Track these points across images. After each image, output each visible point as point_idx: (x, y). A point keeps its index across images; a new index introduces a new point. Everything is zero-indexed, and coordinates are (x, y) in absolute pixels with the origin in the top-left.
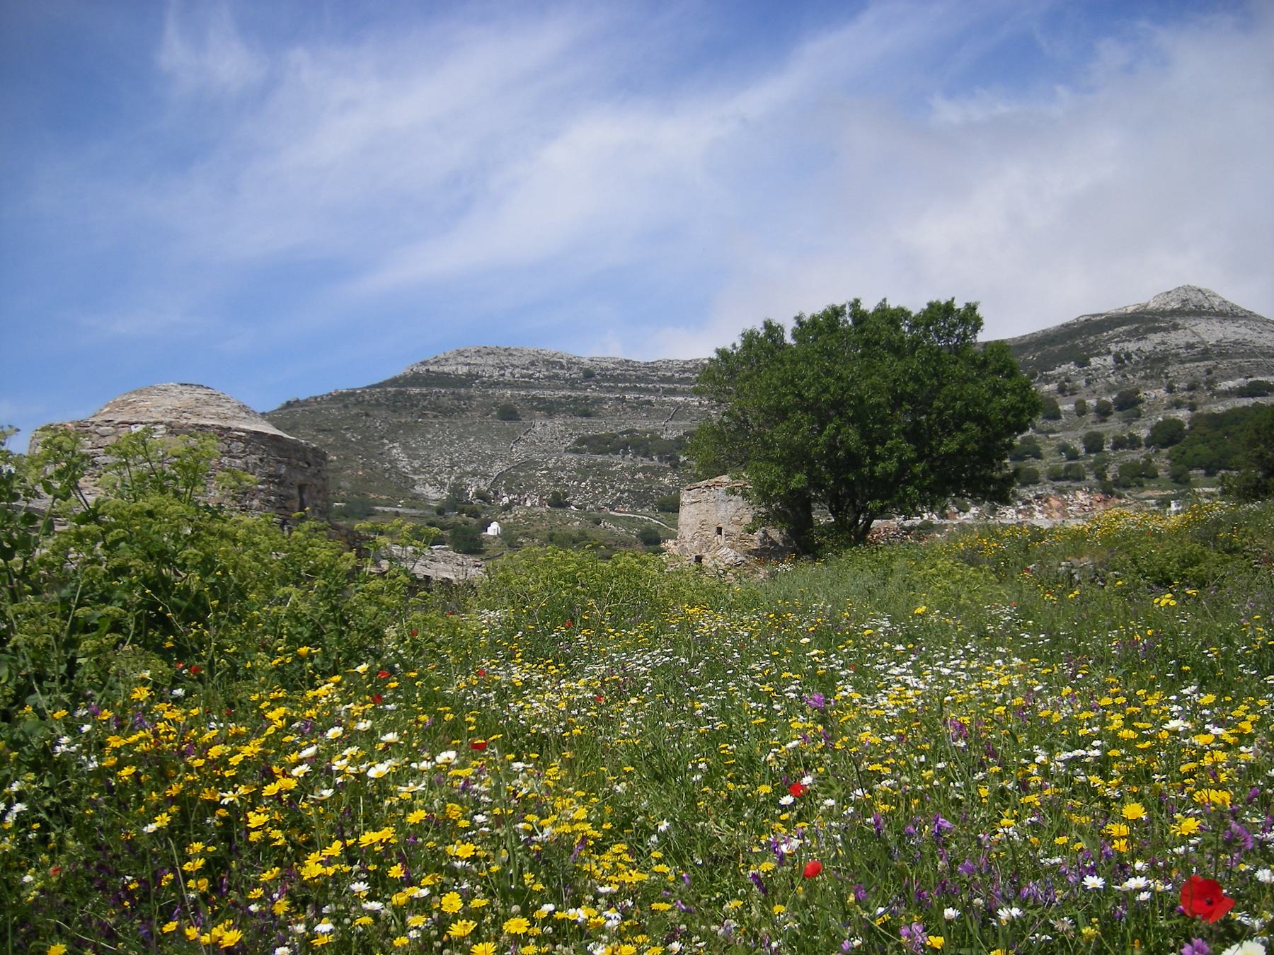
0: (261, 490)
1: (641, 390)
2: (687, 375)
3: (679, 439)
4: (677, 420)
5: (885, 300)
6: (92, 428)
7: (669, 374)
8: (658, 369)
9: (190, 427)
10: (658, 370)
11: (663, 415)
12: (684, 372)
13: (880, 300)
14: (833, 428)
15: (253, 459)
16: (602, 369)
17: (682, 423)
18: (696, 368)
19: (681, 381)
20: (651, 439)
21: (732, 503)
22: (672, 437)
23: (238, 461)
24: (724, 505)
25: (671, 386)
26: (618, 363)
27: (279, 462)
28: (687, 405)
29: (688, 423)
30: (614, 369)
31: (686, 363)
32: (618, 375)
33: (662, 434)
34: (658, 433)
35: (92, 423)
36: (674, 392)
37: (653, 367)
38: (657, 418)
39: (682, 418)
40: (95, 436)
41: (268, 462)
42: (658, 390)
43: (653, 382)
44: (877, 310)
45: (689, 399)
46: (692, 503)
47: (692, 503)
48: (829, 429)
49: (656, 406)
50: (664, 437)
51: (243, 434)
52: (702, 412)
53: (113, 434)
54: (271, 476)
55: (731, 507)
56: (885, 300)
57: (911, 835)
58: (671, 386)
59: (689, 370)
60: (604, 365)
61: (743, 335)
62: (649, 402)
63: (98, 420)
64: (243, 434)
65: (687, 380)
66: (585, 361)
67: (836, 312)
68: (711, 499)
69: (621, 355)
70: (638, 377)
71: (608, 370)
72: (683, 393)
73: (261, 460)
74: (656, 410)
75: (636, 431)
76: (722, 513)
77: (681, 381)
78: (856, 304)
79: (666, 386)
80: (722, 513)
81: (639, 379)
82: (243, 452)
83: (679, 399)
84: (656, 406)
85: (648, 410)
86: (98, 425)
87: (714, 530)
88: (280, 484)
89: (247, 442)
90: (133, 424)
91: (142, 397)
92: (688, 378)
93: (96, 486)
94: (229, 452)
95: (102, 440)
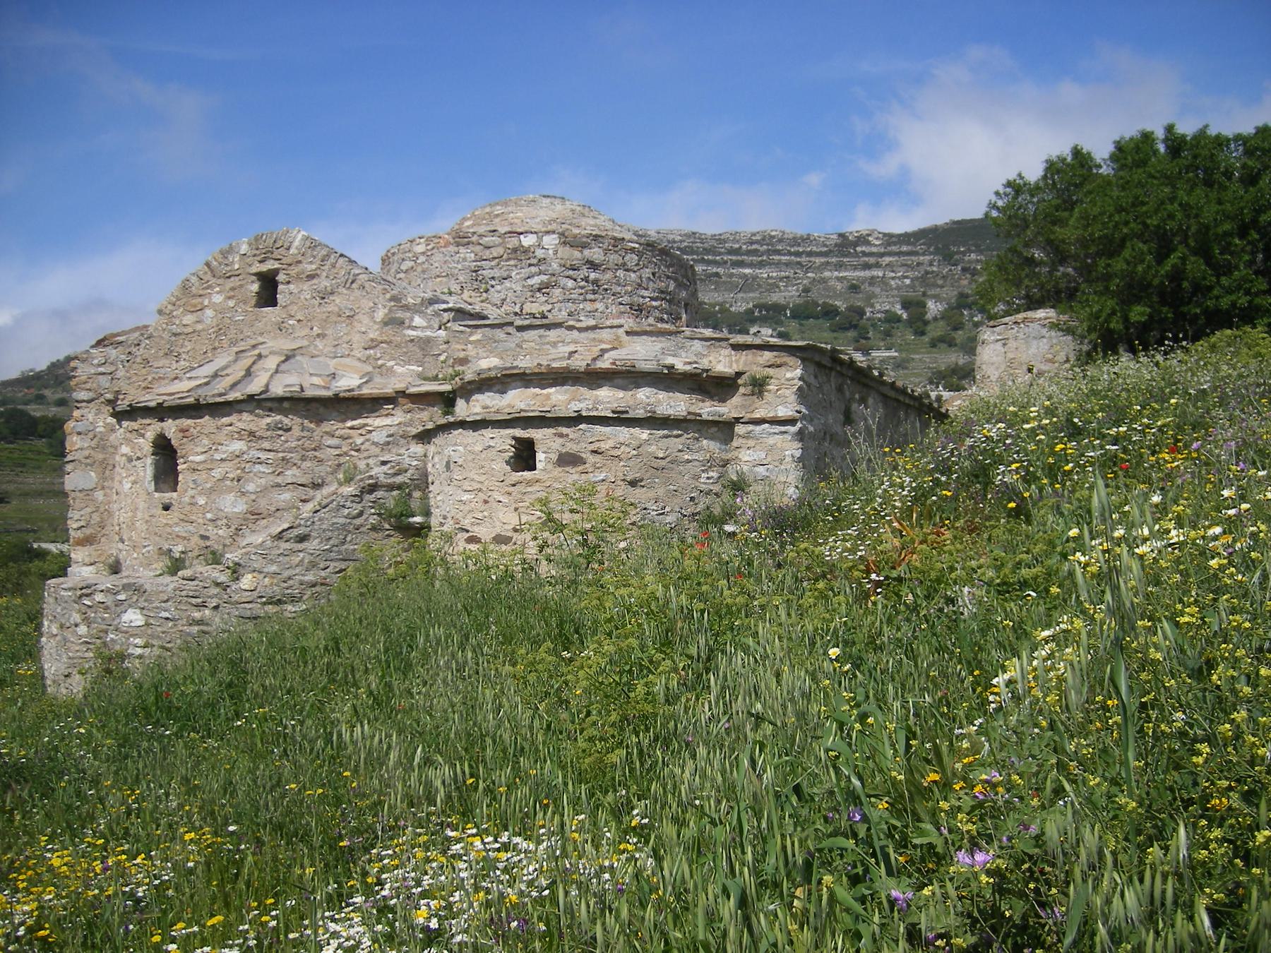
0: (656, 308)
1: (709, 263)
2: (754, 247)
3: (749, 312)
4: (745, 292)
5: (1206, 126)
6: (475, 239)
7: (737, 246)
8: (725, 241)
9: (584, 236)
10: (725, 242)
11: (732, 287)
12: (752, 243)
13: (1200, 126)
14: (1180, 258)
15: (647, 273)
16: (669, 242)
17: (751, 295)
18: (763, 240)
19: (749, 253)
20: (721, 311)
21: (1045, 340)
22: (742, 309)
23: (633, 275)
24: (1035, 342)
25: (739, 258)
26: (685, 235)
27: (668, 277)
28: (755, 278)
29: (756, 295)
30: (681, 241)
31: (754, 235)
32: (686, 247)
33: (731, 306)
34: (728, 306)
35: (474, 233)
36: (741, 264)
37: (721, 240)
38: (725, 290)
39: (751, 290)
40: (478, 248)
41: (660, 277)
42: (726, 262)
43: (720, 254)
44: (1195, 137)
45: (758, 271)
46: (997, 341)
47: (997, 341)
48: (1173, 259)
49: (724, 278)
50: (733, 309)
51: (637, 246)
52: (771, 284)
53: (500, 245)
54: (662, 292)
55: (1044, 345)
56: (1206, 126)
57: (613, 725)
58: (739, 258)
59: (757, 242)
60: (671, 237)
61: (1047, 161)
62: (717, 275)
63: (481, 230)
64: (637, 246)
65: (755, 252)
66: (652, 233)
67: (1147, 137)
68: (1021, 335)
69: (689, 227)
70: (705, 249)
71: (674, 242)
72: (751, 265)
73: (654, 274)
74: (724, 283)
75: (705, 304)
76: (1033, 350)
77: (749, 253)
78: (1170, 129)
79: (734, 258)
80: (1033, 350)
81: (707, 251)
82: (637, 265)
83: (747, 271)
84: (724, 278)
85: (716, 282)
86: (481, 236)
87: (1025, 368)
88: (670, 301)
89: (640, 254)
90: (522, 233)
91: (510, 209)
92: (756, 250)
93: (482, 302)
94: (624, 264)
95: (487, 252)
